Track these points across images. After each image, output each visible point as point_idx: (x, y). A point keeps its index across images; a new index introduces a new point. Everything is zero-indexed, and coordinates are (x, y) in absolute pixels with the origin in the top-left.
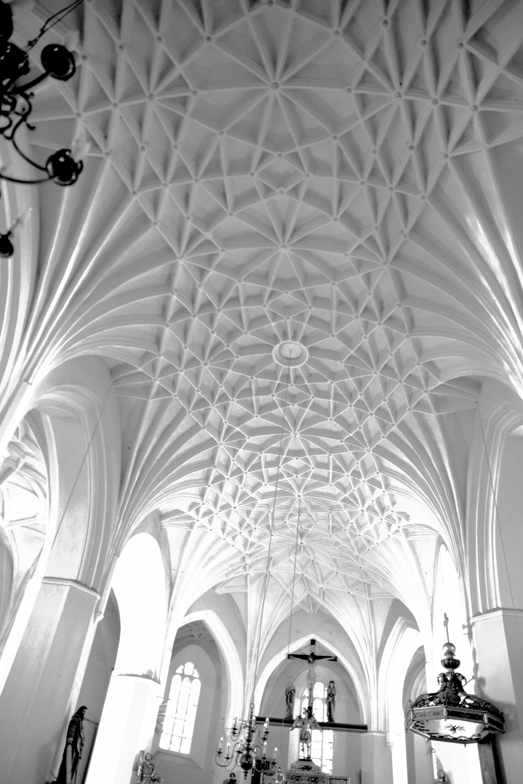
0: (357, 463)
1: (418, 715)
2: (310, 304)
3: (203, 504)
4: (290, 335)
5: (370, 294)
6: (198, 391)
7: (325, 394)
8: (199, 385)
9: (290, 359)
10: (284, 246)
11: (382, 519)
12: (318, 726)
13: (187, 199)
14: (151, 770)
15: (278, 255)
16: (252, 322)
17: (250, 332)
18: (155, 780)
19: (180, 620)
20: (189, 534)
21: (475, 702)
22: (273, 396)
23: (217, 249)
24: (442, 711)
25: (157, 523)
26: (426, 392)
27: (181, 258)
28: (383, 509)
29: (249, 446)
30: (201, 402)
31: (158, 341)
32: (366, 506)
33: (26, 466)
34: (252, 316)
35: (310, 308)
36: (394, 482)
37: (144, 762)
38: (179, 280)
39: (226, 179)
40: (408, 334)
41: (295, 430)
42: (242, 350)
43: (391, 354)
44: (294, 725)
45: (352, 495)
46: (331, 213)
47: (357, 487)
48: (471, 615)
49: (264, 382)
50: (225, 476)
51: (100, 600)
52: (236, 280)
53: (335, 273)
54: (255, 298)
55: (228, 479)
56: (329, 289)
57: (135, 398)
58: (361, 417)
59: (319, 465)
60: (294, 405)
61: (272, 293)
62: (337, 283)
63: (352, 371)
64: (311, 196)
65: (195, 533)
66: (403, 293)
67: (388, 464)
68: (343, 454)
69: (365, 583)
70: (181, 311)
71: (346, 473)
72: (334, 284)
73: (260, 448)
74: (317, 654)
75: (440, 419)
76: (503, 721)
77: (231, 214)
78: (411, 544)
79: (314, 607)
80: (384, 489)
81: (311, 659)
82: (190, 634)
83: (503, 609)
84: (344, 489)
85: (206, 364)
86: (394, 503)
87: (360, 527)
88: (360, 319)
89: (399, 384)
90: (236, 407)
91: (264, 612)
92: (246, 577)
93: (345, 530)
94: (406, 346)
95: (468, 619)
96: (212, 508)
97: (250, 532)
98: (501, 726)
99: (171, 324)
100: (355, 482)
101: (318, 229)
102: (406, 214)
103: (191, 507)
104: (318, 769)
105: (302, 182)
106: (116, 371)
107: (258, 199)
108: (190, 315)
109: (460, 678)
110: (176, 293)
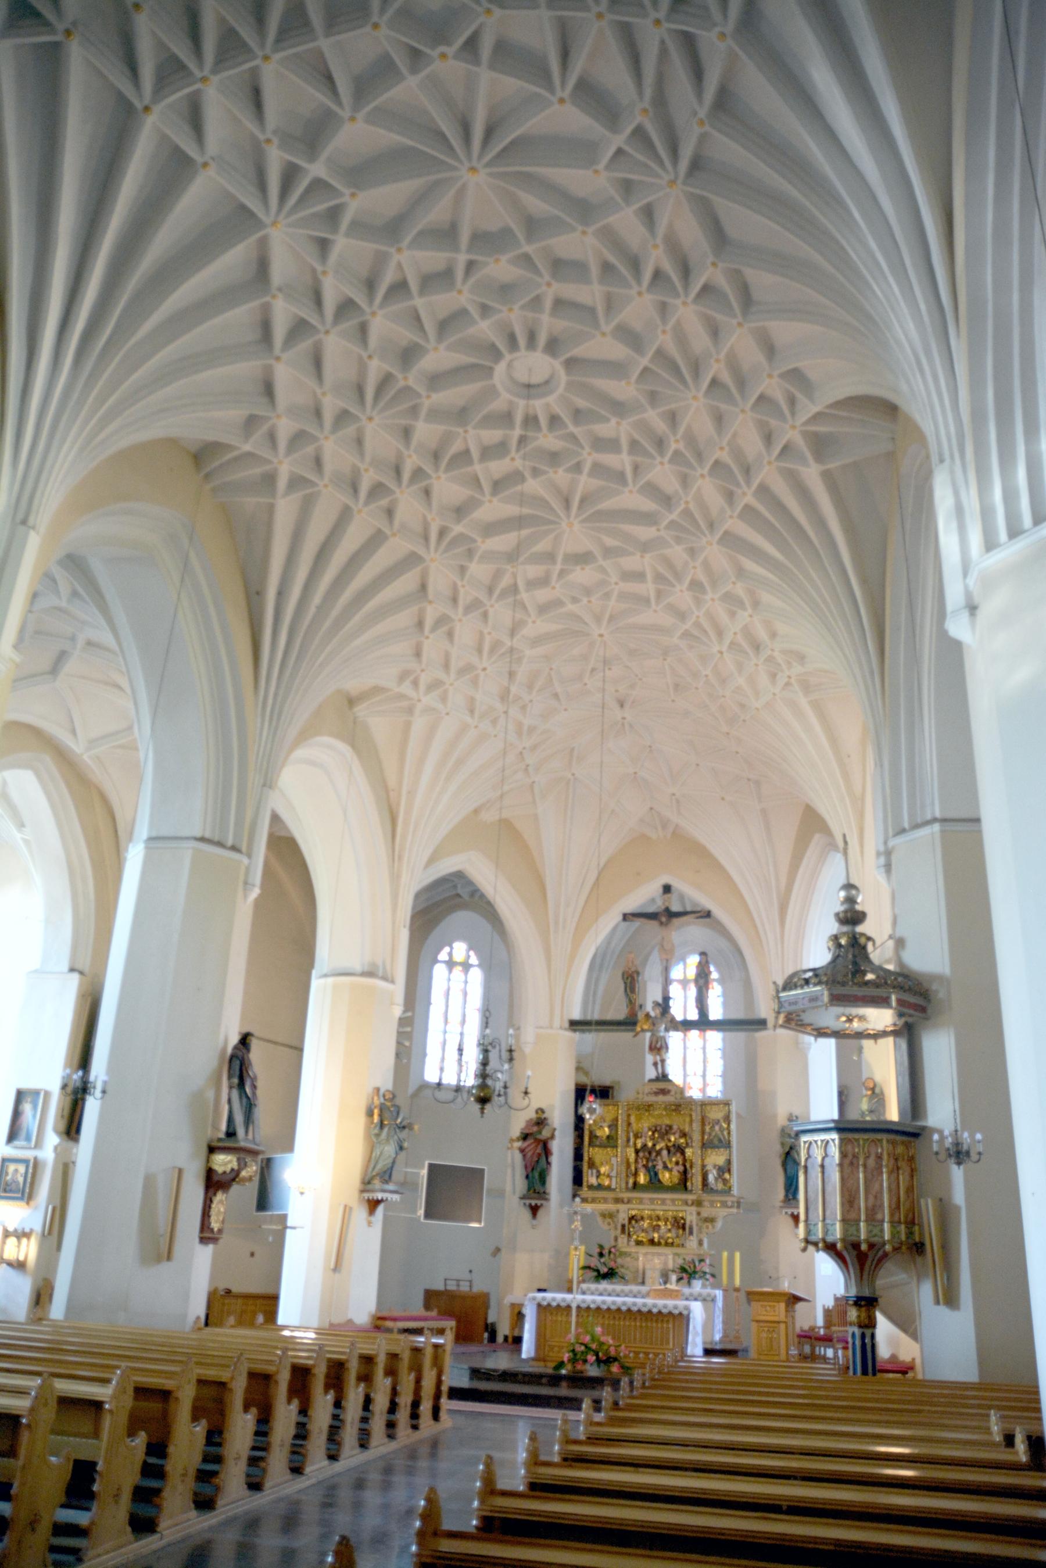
0: (694, 567)
1: (786, 1005)
2: (547, 278)
3: (423, 671)
4: (522, 341)
5: (656, 246)
6: (366, 470)
7: (611, 445)
8: (368, 459)
9: (529, 386)
10: (473, 169)
11: (757, 665)
12: (680, 1027)
13: (256, 98)
14: (395, 1114)
15: (464, 187)
16: (444, 326)
17: (442, 347)
18: (404, 1127)
19: (416, 878)
20: (408, 725)
21: (878, 977)
22: (513, 459)
23: (342, 195)
24: (822, 995)
25: (346, 716)
26: (793, 427)
27: (274, 223)
28: (757, 647)
29: (489, 556)
30: (378, 490)
31: (268, 390)
32: (727, 642)
33: (89, 643)
34: (442, 315)
35: (549, 284)
36: (766, 597)
37: (382, 1104)
38: (280, 269)
39: (325, 44)
40: (740, 319)
41: (568, 517)
42: (436, 380)
43: (717, 361)
44: (638, 1029)
45: (698, 625)
46: (551, 89)
47: (704, 610)
48: (891, 833)
49: (492, 435)
50: (453, 616)
51: (250, 864)
52: (392, 250)
53: (584, 210)
54: (438, 280)
55: (460, 620)
56: (579, 243)
57: (251, 502)
58: (685, 481)
59: (629, 576)
60: (556, 472)
61: (470, 266)
62: (590, 230)
63: (653, 398)
64: (508, 55)
65: (419, 724)
66: (719, 237)
67: (749, 565)
68: (667, 552)
69: (749, 780)
70: (299, 328)
71: (678, 587)
72: (584, 233)
73: (512, 557)
74: (675, 908)
75: (828, 477)
76: (929, 1001)
77: (352, 119)
78: (818, 708)
79: (664, 827)
80: (750, 611)
81: (664, 919)
82: (454, 892)
83: (944, 820)
84: (682, 616)
85: (370, 419)
86: (773, 635)
87: (723, 681)
88: (648, 298)
89: (741, 416)
90: (447, 488)
91: (571, 846)
92: (532, 785)
93: (697, 688)
94: (740, 340)
95: (885, 843)
96: (441, 675)
97: (523, 708)
98: (923, 1010)
99: (285, 356)
100: (698, 602)
101: (535, 124)
102: (698, 73)
103: (403, 677)
104: (681, 1091)
105: (481, 26)
106: (202, 456)
107: (399, 77)
108: (317, 331)
109: (862, 940)
110: (280, 295)
